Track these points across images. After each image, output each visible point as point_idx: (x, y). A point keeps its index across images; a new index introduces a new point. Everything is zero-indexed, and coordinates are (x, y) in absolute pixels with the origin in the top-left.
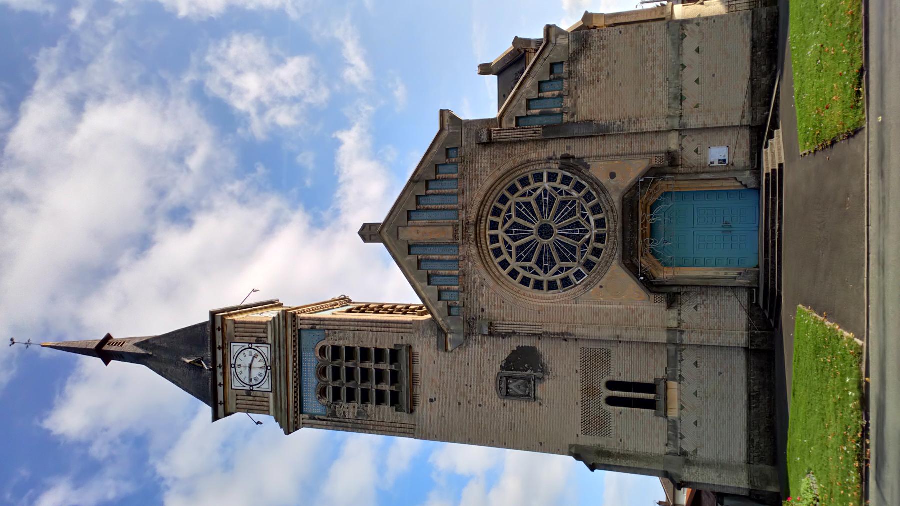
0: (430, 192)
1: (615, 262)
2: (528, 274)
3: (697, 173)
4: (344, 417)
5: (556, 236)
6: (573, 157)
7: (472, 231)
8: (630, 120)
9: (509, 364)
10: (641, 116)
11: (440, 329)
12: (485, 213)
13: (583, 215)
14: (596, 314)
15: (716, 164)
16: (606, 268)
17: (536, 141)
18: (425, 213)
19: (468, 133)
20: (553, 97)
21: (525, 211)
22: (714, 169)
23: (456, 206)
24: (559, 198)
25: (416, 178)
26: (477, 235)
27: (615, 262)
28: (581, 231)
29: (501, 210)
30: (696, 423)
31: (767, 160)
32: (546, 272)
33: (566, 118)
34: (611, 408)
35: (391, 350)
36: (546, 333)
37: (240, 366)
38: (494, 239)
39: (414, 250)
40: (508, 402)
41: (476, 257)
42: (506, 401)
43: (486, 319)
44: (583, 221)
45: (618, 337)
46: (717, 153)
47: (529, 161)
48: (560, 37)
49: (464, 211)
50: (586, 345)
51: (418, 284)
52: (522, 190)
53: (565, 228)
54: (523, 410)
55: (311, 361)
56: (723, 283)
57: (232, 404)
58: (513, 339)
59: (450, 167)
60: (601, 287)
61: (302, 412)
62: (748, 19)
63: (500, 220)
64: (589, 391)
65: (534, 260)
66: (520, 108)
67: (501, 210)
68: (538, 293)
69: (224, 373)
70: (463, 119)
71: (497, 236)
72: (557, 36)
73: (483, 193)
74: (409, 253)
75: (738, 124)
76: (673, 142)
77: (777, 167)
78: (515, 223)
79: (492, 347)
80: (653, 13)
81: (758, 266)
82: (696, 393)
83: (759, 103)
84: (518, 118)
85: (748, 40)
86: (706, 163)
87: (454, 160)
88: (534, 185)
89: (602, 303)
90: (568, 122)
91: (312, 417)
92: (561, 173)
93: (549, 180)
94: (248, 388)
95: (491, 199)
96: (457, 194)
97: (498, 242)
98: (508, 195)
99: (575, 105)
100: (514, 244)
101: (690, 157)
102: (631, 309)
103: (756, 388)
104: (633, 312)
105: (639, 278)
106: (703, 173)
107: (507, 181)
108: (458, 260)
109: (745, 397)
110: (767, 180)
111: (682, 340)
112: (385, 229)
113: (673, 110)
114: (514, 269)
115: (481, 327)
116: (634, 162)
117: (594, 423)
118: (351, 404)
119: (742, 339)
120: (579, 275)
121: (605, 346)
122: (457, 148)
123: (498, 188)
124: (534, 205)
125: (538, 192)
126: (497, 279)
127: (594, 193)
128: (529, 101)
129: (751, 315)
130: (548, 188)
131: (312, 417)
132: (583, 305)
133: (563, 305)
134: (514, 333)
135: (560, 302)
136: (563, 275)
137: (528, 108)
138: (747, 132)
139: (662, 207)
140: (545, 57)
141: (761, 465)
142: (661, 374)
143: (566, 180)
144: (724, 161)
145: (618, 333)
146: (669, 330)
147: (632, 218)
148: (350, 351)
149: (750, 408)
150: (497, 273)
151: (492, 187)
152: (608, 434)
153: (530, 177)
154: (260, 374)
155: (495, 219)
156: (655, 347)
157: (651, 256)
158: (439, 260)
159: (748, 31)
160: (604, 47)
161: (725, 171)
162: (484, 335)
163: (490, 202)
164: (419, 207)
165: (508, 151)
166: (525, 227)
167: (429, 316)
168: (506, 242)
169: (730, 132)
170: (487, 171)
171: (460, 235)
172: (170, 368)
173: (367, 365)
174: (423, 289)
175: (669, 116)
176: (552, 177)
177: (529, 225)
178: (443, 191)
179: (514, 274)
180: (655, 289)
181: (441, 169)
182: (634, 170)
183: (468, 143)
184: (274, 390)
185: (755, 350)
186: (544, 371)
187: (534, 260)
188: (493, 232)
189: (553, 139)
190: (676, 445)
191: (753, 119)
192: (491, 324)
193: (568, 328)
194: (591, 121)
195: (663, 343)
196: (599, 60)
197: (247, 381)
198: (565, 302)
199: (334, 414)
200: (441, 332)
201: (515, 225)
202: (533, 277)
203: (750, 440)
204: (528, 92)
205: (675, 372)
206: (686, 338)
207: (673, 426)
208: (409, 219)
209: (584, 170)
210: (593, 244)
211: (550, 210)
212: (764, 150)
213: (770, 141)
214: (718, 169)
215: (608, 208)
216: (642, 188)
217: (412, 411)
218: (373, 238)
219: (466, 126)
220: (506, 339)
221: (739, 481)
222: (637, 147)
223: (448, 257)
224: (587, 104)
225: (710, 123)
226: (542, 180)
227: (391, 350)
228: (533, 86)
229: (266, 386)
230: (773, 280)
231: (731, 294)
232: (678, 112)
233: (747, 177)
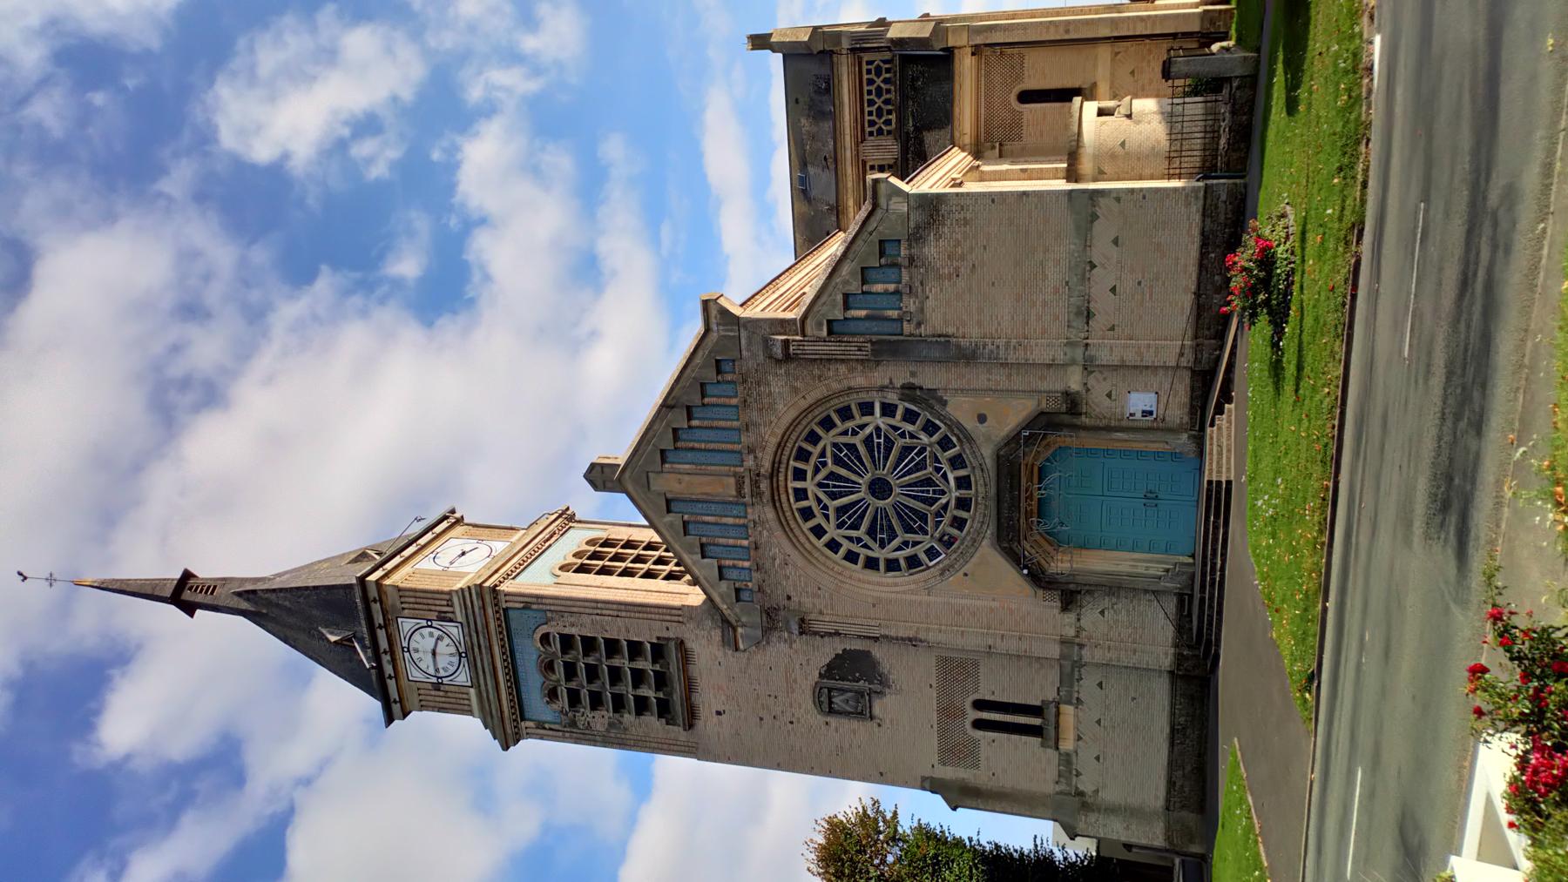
0: (695, 423)
2: (855, 548)
4: (589, 726)
6: (921, 388)
7: (766, 485)
9: (830, 671)
13: (938, 470)
14: (959, 613)
15: (1139, 416)
19: (749, 339)
20: (886, 293)
21: (847, 456)
22: (1135, 424)
23: (737, 447)
24: (900, 443)
25: (670, 402)
26: (774, 490)
29: (810, 454)
30: (1098, 758)
32: (882, 546)
33: (907, 328)
34: (979, 734)
35: (652, 644)
36: (886, 637)
37: (417, 651)
38: (801, 494)
40: (833, 720)
41: (774, 524)
42: (829, 719)
44: (937, 477)
46: (1139, 402)
48: (894, 199)
54: (854, 732)
55: (529, 654)
57: (412, 698)
58: (837, 639)
61: (523, 719)
62: (1197, 198)
64: (948, 712)
66: (834, 306)
67: (810, 454)
68: (871, 575)
69: (394, 661)
71: (805, 491)
72: (889, 198)
73: (780, 432)
74: (669, 511)
76: (1074, 382)
78: (832, 473)
80: (1052, 29)
82: (1099, 722)
84: (829, 322)
85: (1196, 232)
87: (729, 377)
88: (859, 420)
91: (540, 725)
93: (884, 414)
94: (434, 680)
95: (793, 437)
99: (922, 310)
101: (1098, 402)
103: (1182, 720)
104: (1011, 611)
108: (745, 526)
109: (1167, 730)
112: (627, 474)
117: (952, 751)
118: (597, 714)
119: (1166, 660)
120: (932, 554)
124: (862, 449)
126: (807, 555)
127: (954, 439)
128: (846, 296)
131: (540, 725)
132: (939, 600)
133: (908, 597)
134: (837, 634)
136: (908, 552)
137: (847, 307)
138: (1187, 375)
140: (870, 229)
141: (1184, 813)
142: (1051, 695)
143: (910, 417)
144: (1151, 413)
145: (990, 642)
146: (1064, 642)
148: (589, 644)
149: (1172, 744)
150: (807, 545)
151: (795, 423)
152: (976, 766)
153: (853, 407)
154: (451, 663)
158: (716, 524)
159: (1197, 218)
160: (966, 222)
164: (679, 444)
166: (847, 480)
170: (785, 401)
171: (747, 489)
172: (302, 637)
173: (616, 662)
174: (694, 563)
176: (888, 410)
177: (853, 477)
178: (715, 423)
179: (833, 546)
182: (1012, 415)
183: (751, 357)
184: (475, 684)
185: (1182, 677)
186: (884, 682)
188: (799, 485)
190: (1069, 784)
192: (802, 620)
196: (958, 243)
197: (431, 671)
198: (913, 592)
199: (573, 724)
200: (727, 624)
202: (863, 552)
203: (1171, 784)
204: (846, 283)
205: (1070, 694)
207: (1067, 760)
208: (663, 461)
209: (937, 407)
211: (886, 458)
212: (1209, 430)
214: (1140, 425)
217: (691, 726)
218: (609, 485)
221: (1152, 835)
223: (730, 521)
224: (941, 310)
225: (1131, 357)
227: (652, 644)
228: (852, 273)
229: (463, 678)
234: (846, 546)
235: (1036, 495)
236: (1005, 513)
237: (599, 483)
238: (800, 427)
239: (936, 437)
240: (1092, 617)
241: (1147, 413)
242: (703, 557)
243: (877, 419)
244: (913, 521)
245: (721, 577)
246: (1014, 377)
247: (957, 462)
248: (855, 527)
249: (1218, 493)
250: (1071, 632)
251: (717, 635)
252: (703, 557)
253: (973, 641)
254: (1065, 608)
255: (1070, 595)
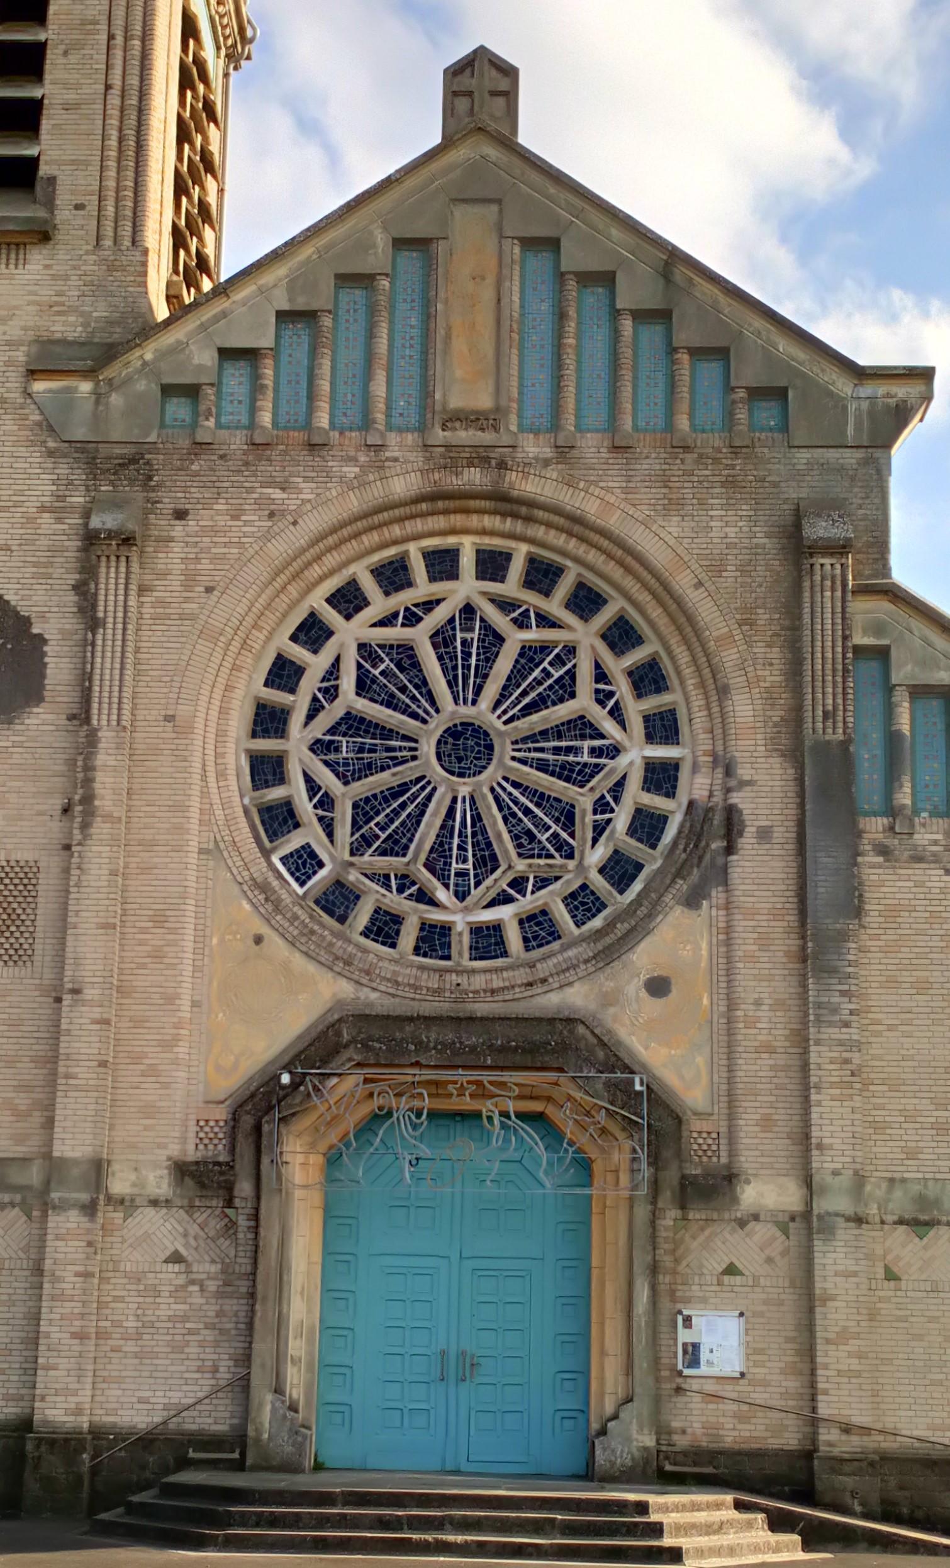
0: (627, 324)
1: (345, 989)
2: (309, 684)
3: (654, 1269)
5: (448, 787)
6: (730, 850)
7: (473, 481)
8: (856, 1046)
10: (866, 1085)
11: (110, 353)
12: (540, 532)
13: (518, 884)
14: (160, 920)
15: (684, 1336)
16: (324, 957)
17: (795, 718)
18: (545, 307)
19: (841, 469)
21: (543, 676)
22: (664, 1329)
23: (569, 421)
24: (583, 800)
25: (680, 273)
27: (345, 989)
28: (462, 874)
31: (695, 1507)
32: (318, 747)
33: (874, 827)
38: (443, 564)
39: (409, 261)
41: (376, 493)
43: (146, 524)
44: (498, 881)
45: (76, 991)
46: (720, 1340)
47: (723, 691)
49: (548, 452)
50: (47, 884)
51: (280, 271)
52: (618, 667)
53: (477, 818)
56: (262, 1348)
59: (716, 403)
60: (258, 940)
63: (511, 586)
65: (363, 706)
68: (240, 718)
70: (894, 451)
71: (453, 574)
73: (613, 522)
74: (400, 243)
75: (823, 1411)
76: (766, 1191)
77: (667, 1541)
78: (500, 639)
79: (44, 542)
81: (318, 1467)
83: (893, 1482)
84: (882, 654)
86: (687, 1301)
87: (742, 415)
88: (635, 709)
89: (201, 939)
90: (859, 834)
92: (674, 809)
95: (592, 556)
96: (612, 424)
97: (432, 579)
98: (604, 617)
99: (918, 859)
100: (420, 636)
101: (712, 1247)
102: (176, 1039)
104: (168, 1045)
105: (287, 1067)
106: (654, 1288)
107: (656, 613)
108: (367, 423)
110: (621, 1507)
111: (61, 1207)
112: (492, 152)
113: (880, 1193)
114: (330, 634)
115: (116, 505)
116: (701, 1060)
119: (62, 1407)
120: (304, 863)
121: (43, 949)
122: (784, 428)
123: (629, 583)
125: (609, 726)
126: (294, 569)
127: (597, 922)
129: (147, 1441)
130: (623, 761)
132: (192, 875)
133: (195, 803)
134: (93, 624)
135: (205, 794)
136: (305, 807)
138: (790, 1439)
139: (540, 1149)
143: (647, 826)
145: (90, 993)
146: (98, 1168)
147: (503, 1049)
150: (316, 570)
151: (629, 557)
155: (517, 568)
156: (37, 1118)
157: (365, 1109)
161: (656, 1361)
162: (87, 515)
163: (581, 550)
164: (572, 284)
165: (763, 617)
166: (483, 676)
167: (162, 312)
168: (429, 605)
169: (793, 1384)
170: (690, 542)
171: (464, 436)
175: (860, 1179)
176: (662, 777)
177: (492, 690)
178: (627, 375)
180: (247, 1121)
181: (711, 371)
182: (671, 1054)
187: (363, 706)
188: (467, 562)
189: (800, 781)
191: (838, 1463)
192: (128, 541)
193: (108, 818)
194: (858, 912)
195: (49, 1143)
198: (207, 812)
200: (99, 355)
201: (493, 640)
206: (67, 1223)
208: (529, 243)
209: (682, 886)
210: (414, 915)
211: (542, 766)
212: (729, 1498)
213: (760, 1517)
215: (543, 969)
216: (610, 1085)
218: (462, 104)
219: (866, 462)
220: (72, 598)
222: (755, 1069)
223: (379, 387)
225: (833, 1318)
226: (650, 738)
227: (33, 163)
230: (260, 1521)
231: (224, 1375)
232: (873, 1210)
233: (635, 1438)
234: (316, 664)
235: (486, 1107)
236: (432, 1035)
237: (466, 81)
238: (617, 573)
239: (599, 883)
240: (158, 1235)
241: (693, 1353)
242: (281, 315)
243: (636, 753)
244: (383, 823)
245: (226, 354)
246: (766, 1060)
247: (539, 929)
248: (363, 686)
249: (631, 1530)
250: (119, 1185)
251: (67, 327)
252: (281, 315)
253: (91, 953)
254: (182, 1170)
255: (227, 1176)
